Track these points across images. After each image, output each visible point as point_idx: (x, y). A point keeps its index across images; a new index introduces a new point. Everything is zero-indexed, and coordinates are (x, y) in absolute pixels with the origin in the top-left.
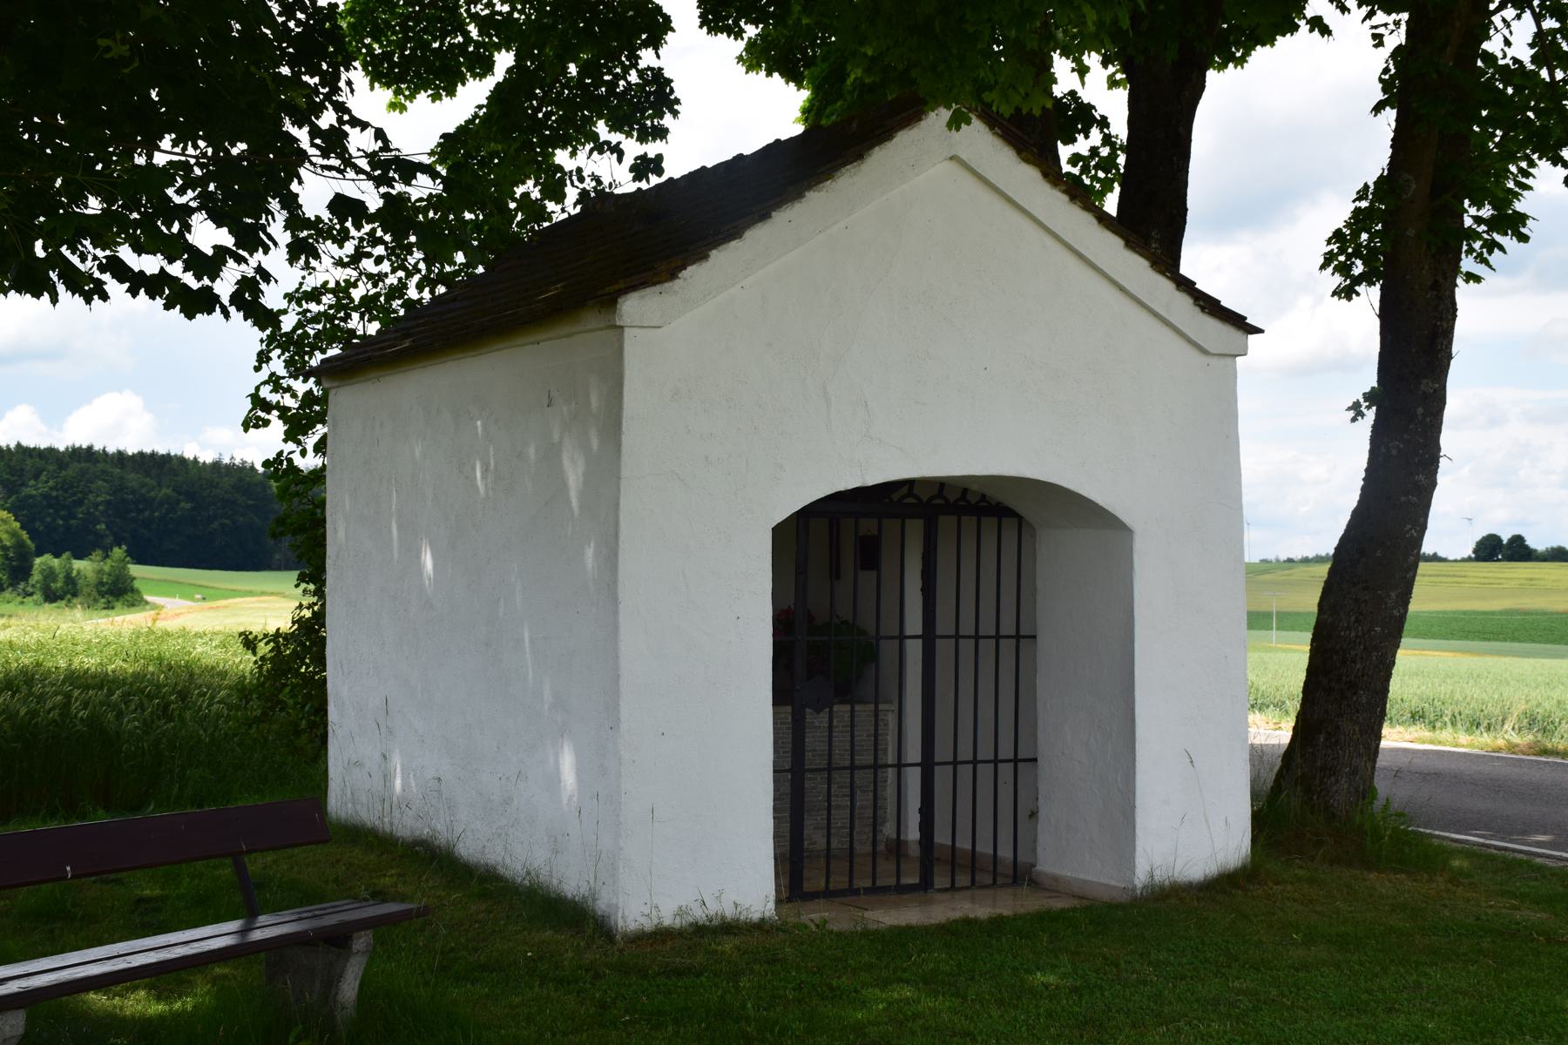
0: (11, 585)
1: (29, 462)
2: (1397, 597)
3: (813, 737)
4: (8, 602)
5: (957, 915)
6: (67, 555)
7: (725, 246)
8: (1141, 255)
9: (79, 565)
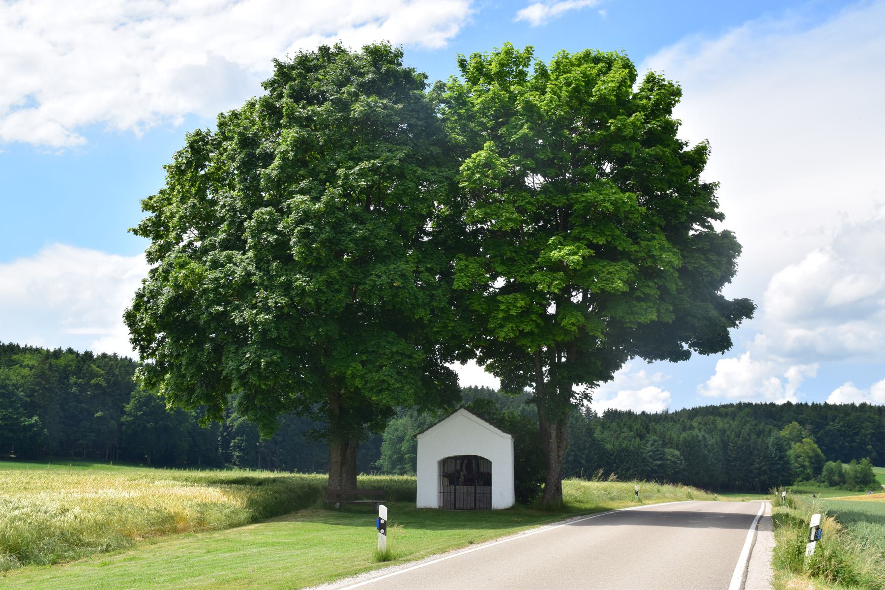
0: (814, 477)
1: (830, 412)
4: (813, 486)
5: (267, 476)
6: (839, 461)
9: (846, 467)
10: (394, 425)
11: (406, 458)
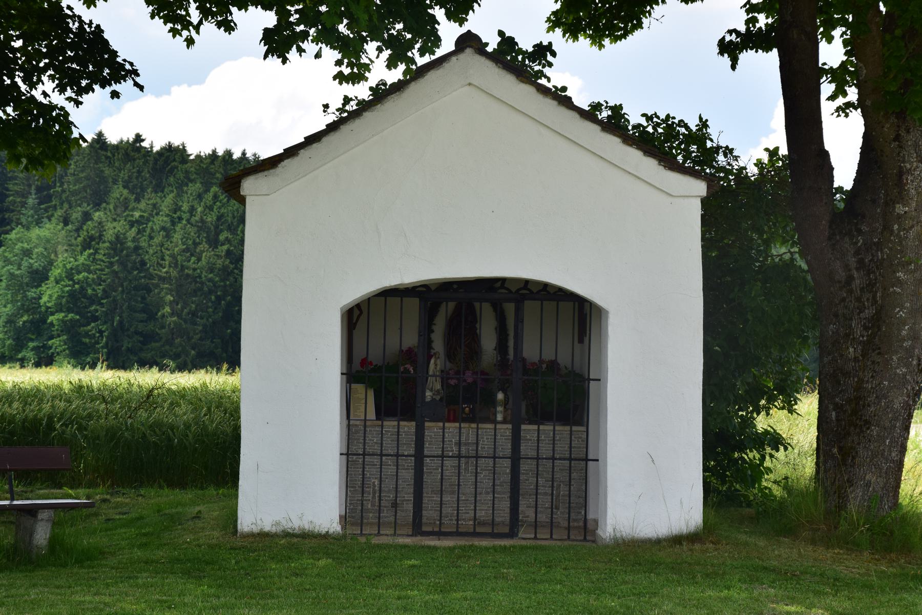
2: (898, 360)
3: (525, 446)
7: (309, 147)
8: (615, 135)
10: (19, 240)
11: (52, 324)
